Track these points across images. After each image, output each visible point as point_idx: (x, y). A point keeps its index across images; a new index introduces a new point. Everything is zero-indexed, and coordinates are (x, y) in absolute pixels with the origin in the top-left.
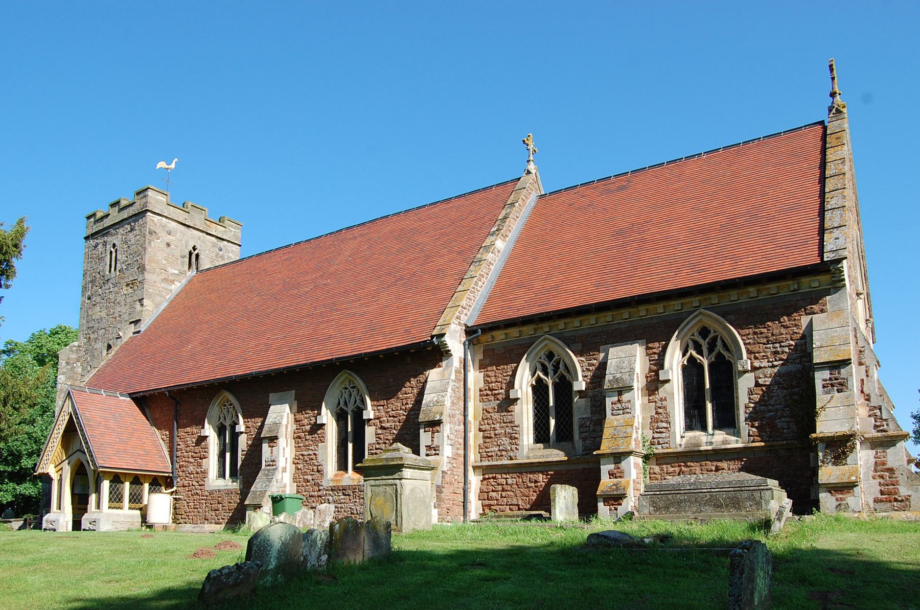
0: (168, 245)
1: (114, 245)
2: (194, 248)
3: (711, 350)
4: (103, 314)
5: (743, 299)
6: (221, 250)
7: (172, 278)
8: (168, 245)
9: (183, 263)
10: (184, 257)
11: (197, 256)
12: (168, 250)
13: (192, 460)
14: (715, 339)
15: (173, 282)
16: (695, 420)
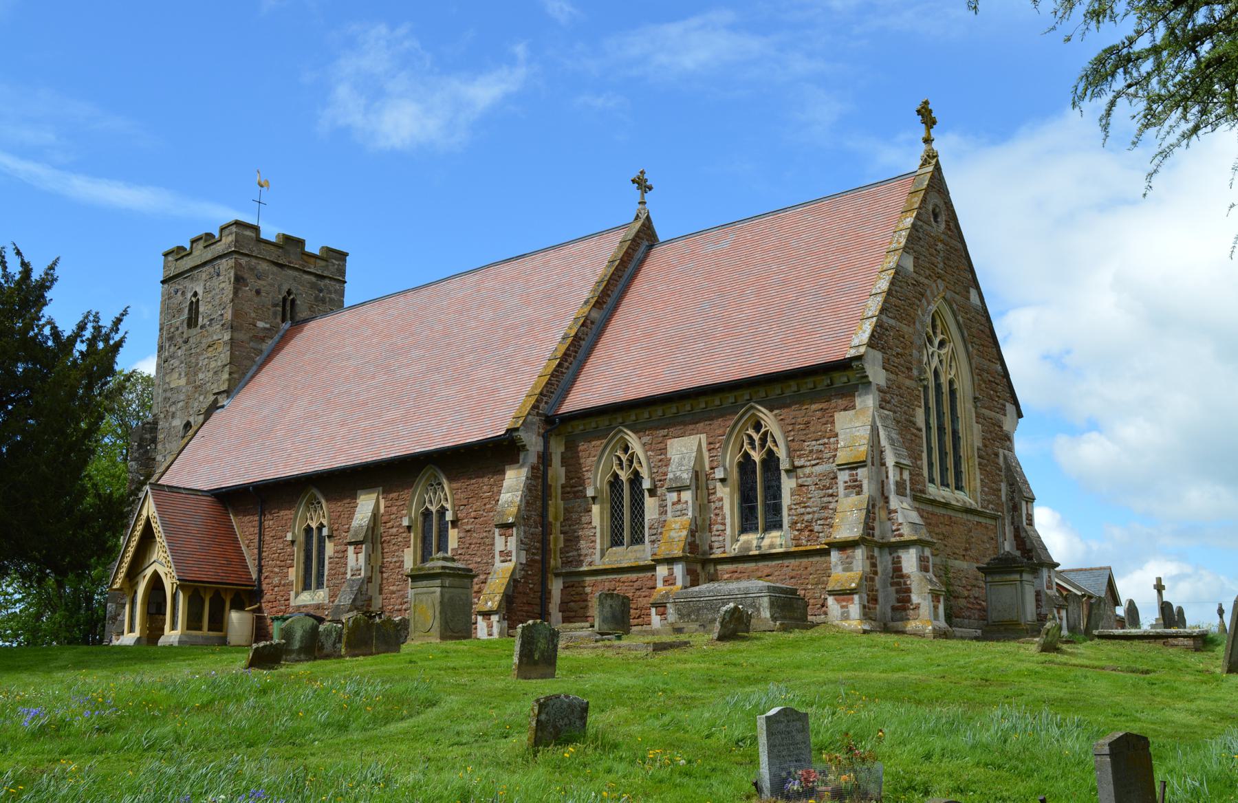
0: (258, 292)
1: (195, 294)
2: (289, 293)
3: (763, 446)
4: (183, 382)
5: (160, 529)
6: (321, 291)
7: (261, 334)
8: (258, 292)
9: (275, 314)
10: (275, 305)
11: (293, 301)
12: (256, 300)
13: (276, 570)
14: (766, 433)
15: (263, 340)
16: (747, 523)
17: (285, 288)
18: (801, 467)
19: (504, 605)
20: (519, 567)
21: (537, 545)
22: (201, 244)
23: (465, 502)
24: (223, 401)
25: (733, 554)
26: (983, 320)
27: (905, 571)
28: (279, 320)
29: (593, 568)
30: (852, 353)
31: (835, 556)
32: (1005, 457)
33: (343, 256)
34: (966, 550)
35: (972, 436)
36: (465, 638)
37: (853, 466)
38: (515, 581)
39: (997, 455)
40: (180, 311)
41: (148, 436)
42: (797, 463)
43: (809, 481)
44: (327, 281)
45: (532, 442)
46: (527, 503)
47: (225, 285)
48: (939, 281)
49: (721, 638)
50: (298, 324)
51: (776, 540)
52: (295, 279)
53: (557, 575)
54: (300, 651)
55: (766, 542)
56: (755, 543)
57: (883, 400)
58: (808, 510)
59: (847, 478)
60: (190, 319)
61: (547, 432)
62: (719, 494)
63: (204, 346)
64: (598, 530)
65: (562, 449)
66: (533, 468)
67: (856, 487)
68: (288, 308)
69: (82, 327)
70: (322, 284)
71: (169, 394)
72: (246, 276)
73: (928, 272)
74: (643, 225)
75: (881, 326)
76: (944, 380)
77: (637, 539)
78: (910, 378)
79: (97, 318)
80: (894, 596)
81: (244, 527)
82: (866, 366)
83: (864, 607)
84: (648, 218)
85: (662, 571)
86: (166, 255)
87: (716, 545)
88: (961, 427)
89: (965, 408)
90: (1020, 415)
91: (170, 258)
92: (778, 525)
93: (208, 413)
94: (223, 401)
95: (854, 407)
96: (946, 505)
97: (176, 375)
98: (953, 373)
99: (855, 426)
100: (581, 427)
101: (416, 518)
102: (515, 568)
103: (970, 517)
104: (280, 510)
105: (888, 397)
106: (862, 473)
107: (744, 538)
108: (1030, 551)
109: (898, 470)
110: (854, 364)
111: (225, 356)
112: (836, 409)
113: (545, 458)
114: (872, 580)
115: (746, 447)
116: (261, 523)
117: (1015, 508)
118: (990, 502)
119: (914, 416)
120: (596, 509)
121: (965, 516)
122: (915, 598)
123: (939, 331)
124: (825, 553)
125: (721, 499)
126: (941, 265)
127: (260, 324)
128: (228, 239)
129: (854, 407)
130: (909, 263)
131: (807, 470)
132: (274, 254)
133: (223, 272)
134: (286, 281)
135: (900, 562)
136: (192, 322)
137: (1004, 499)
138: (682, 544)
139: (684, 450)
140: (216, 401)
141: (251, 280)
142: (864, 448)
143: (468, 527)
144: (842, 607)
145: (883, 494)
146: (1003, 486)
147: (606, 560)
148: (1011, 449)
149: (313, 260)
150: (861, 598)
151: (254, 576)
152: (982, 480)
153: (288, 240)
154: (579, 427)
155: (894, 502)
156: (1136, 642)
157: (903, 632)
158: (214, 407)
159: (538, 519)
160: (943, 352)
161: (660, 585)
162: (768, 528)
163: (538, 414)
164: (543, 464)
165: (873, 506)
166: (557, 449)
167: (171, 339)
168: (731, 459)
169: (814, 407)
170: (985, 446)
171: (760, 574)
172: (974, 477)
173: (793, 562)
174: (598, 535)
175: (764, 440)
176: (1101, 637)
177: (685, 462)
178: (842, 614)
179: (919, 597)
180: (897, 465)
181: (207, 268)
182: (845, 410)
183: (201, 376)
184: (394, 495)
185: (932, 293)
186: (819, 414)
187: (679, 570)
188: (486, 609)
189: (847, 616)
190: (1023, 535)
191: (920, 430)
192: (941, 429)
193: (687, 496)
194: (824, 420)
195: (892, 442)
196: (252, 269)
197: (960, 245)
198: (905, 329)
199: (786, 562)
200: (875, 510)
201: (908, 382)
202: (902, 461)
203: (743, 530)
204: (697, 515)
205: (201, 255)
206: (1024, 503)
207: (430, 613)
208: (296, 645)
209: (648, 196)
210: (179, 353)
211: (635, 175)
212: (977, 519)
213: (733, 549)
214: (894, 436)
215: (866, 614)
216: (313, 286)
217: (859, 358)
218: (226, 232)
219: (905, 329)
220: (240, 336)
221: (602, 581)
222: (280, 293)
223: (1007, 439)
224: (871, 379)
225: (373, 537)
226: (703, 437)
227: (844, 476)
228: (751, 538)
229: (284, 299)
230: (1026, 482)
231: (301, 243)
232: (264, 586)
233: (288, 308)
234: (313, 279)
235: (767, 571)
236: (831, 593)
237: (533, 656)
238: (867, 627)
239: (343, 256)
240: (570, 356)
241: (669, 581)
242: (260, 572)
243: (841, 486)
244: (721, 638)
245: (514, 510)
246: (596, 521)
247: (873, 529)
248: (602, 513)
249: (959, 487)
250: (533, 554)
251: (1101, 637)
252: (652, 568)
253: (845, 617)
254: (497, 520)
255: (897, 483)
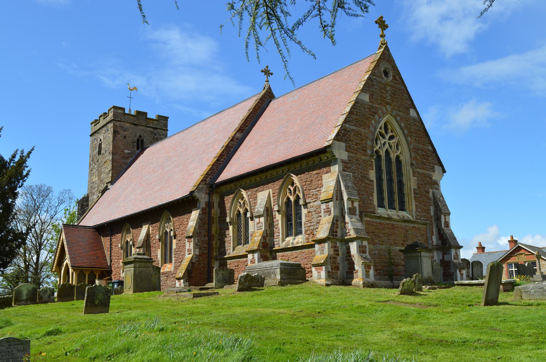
0: (125, 137)
1: (101, 140)
2: (140, 136)
4: (97, 179)
6: (156, 135)
7: (127, 156)
8: (125, 137)
9: (133, 146)
10: (134, 142)
11: (142, 140)
12: (124, 140)
14: (296, 186)
15: (128, 158)
17: (138, 134)
18: (309, 203)
19: (186, 274)
20: (195, 256)
21: (205, 246)
22: (102, 117)
23: (178, 227)
24: (110, 186)
25: (281, 248)
26: (419, 124)
27: (352, 253)
28: (135, 149)
29: (230, 256)
30: (327, 144)
31: (317, 246)
32: (433, 193)
33: (166, 119)
34: (404, 241)
35: (411, 183)
36: (154, 290)
37: (327, 201)
38: (193, 263)
39: (428, 192)
40: (96, 148)
41: (85, 204)
42: (307, 201)
43: (312, 210)
44: (159, 130)
45: (203, 198)
46: (200, 226)
47: (110, 135)
48: (387, 106)
49: (239, 290)
50: (143, 150)
51: (300, 240)
52: (143, 130)
53: (217, 260)
54: (27, 300)
55: (296, 241)
56: (291, 241)
57: (345, 167)
58: (312, 224)
59: (325, 207)
60: (99, 151)
61: (210, 192)
62: (277, 218)
63: (103, 162)
64: (232, 238)
65: (218, 200)
66: (203, 209)
67: (328, 211)
68: (140, 143)
69: (14, 156)
70: (156, 131)
71: (92, 185)
72: (119, 130)
73: (379, 102)
74: (267, 91)
75: (345, 130)
76: (393, 156)
77: (247, 242)
78: (365, 155)
79: (22, 152)
80: (347, 266)
81: (105, 241)
82: (334, 150)
83: (329, 272)
84: (269, 88)
85: (250, 256)
86: (91, 124)
87: (276, 243)
88: (404, 179)
89: (407, 170)
90: (444, 171)
91: (93, 125)
92: (301, 233)
93: (103, 192)
94: (110, 186)
95: (330, 172)
96: (389, 219)
97: (94, 176)
98: (398, 153)
99: (329, 179)
100: (225, 189)
101: (162, 235)
102: (192, 257)
103: (407, 224)
104: (117, 233)
105: (349, 165)
106: (331, 204)
107: (287, 239)
108: (445, 240)
109: (350, 203)
110: (328, 150)
111: (110, 167)
112: (323, 173)
113: (210, 205)
114: (335, 258)
115: (288, 194)
116: (111, 241)
117: (438, 219)
118: (421, 216)
119: (368, 174)
120: (231, 227)
121: (404, 224)
122: (356, 267)
123: (389, 131)
124: (312, 246)
125: (278, 221)
126: (389, 97)
127: (126, 151)
128: (111, 114)
129: (330, 172)
130: (366, 98)
131: (311, 204)
132: (133, 120)
133: (109, 130)
134: (139, 131)
135: (350, 249)
136: (99, 153)
137: (432, 214)
138: (258, 243)
139: (263, 196)
140: (107, 186)
141: (122, 132)
142: (332, 192)
143: (179, 239)
144: (318, 272)
145: (342, 215)
146: (432, 208)
147: (235, 251)
148: (438, 189)
149: (151, 121)
150: (326, 268)
151: (109, 264)
152: (416, 205)
153: (138, 113)
154: (224, 188)
155: (347, 219)
156: (474, 287)
157: (351, 285)
158: (106, 189)
159: (206, 234)
160: (391, 142)
161: (249, 263)
162: (296, 235)
163: (206, 184)
164: (209, 207)
165: (337, 221)
166: (216, 199)
167: (93, 160)
168: (282, 200)
169: (315, 172)
170: (419, 187)
171: (293, 257)
172: (412, 204)
173: (306, 250)
174: (232, 240)
175: (295, 190)
176: (458, 285)
177: (262, 203)
178: (318, 276)
179: (358, 266)
180: (349, 199)
181: (105, 128)
182: (326, 173)
183: (102, 176)
184: (154, 225)
185: (382, 111)
186: (316, 176)
187: (256, 255)
188: (178, 277)
189: (319, 276)
190: (442, 232)
191: (372, 181)
192: (390, 181)
193: (262, 219)
194: (318, 179)
195: (347, 187)
196: (122, 127)
197: (403, 87)
198: (362, 130)
199: (303, 250)
200: (337, 224)
201: (364, 157)
202: (352, 197)
203: (288, 236)
204: (268, 229)
205: (102, 122)
206: (443, 217)
207: (130, 280)
208: (24, 297)
209: (271, 78)
210: (96, 166)
211: (263, 68)
212: (412, 225)
213: (283, 245)
214: (350, 184)
215: (329, 275)
216: (152, 133)
217: (329, 146)
218: (110, 112)
219: (362, 130)
220: (117, 157)
221: (234, 262)
222: (135, 137)
223: (435, 184)
224: (337, 157)
225: (147, 243)
226: (271, 190)
227: (323, 206)
228: (290, 239)
229: (138, 140)
230: (445, 205)
231: (145, 114)
232: (113, 269)
233: (140, 143)
234: (152, 130)
235: (296, 255)
236: (314, 265)
237: (94, 302)
238: (329, 283)
239: (166, 119)
240: (224, 155)
241: (253, 262)
242: (111, 261)
243: (322, 211)
244: (239, 290)
245: (193, 230)
246: (231, 234)
247: (336, 232)
248: (233, 229)
249: (402, 209)
250: (203, 250)
251: (458, 285)
252: (245, 256)
253: (319, 277)
254: (186, 235)
255: (349, 209)
